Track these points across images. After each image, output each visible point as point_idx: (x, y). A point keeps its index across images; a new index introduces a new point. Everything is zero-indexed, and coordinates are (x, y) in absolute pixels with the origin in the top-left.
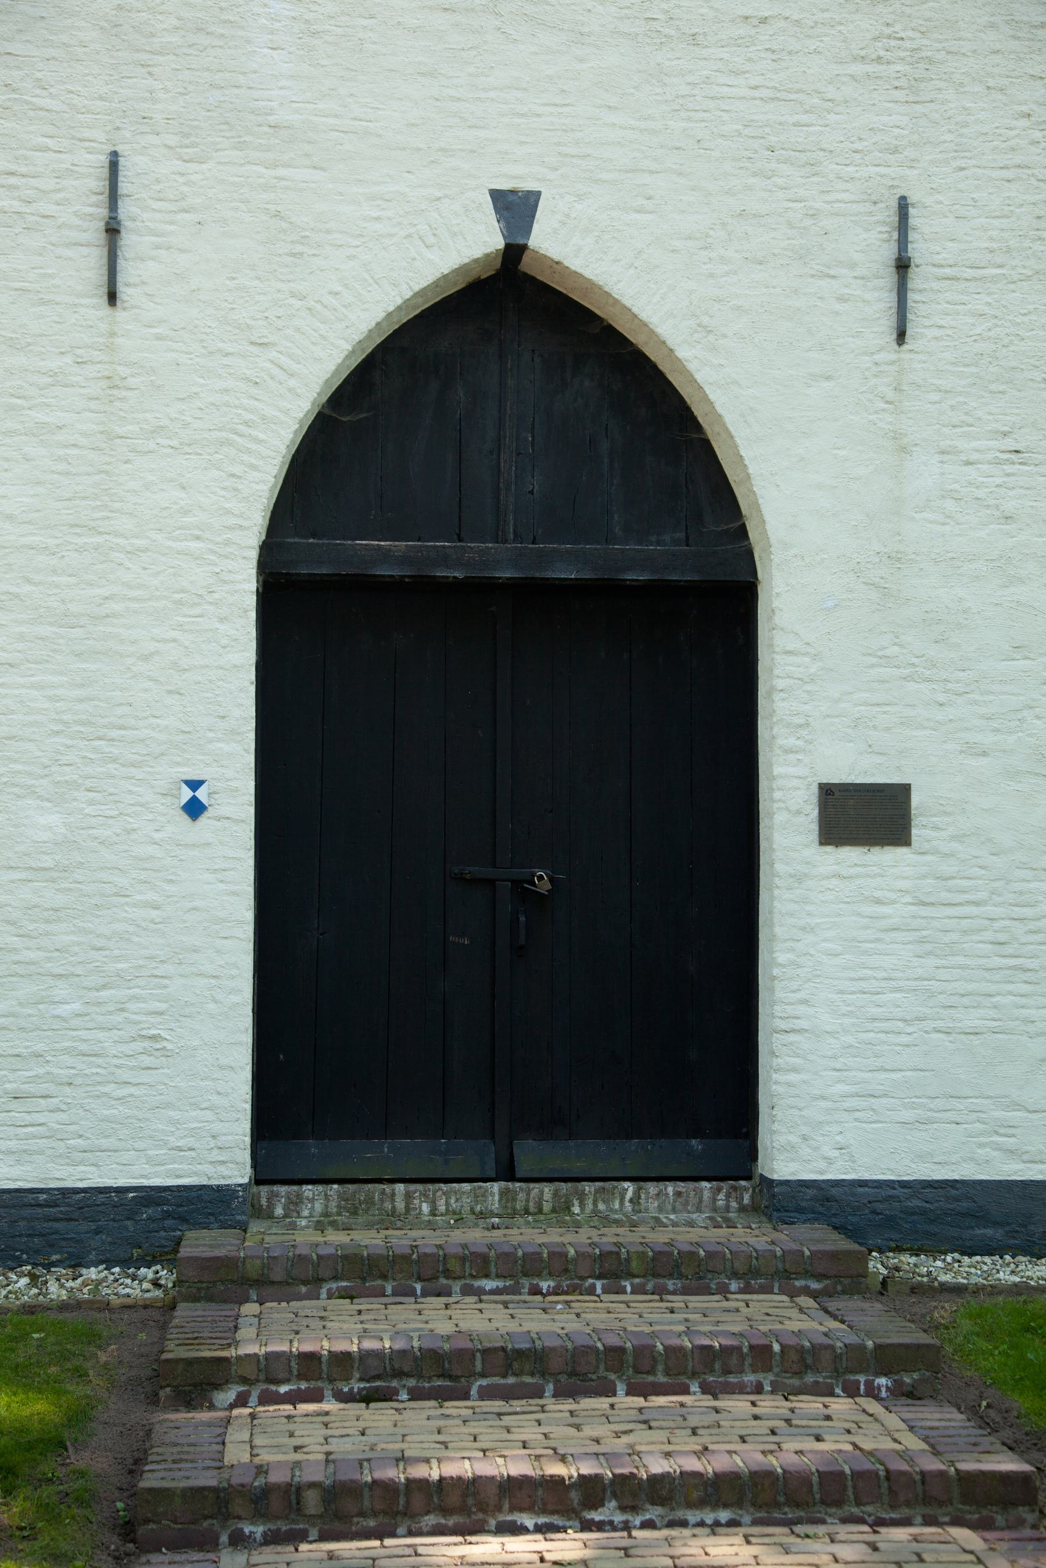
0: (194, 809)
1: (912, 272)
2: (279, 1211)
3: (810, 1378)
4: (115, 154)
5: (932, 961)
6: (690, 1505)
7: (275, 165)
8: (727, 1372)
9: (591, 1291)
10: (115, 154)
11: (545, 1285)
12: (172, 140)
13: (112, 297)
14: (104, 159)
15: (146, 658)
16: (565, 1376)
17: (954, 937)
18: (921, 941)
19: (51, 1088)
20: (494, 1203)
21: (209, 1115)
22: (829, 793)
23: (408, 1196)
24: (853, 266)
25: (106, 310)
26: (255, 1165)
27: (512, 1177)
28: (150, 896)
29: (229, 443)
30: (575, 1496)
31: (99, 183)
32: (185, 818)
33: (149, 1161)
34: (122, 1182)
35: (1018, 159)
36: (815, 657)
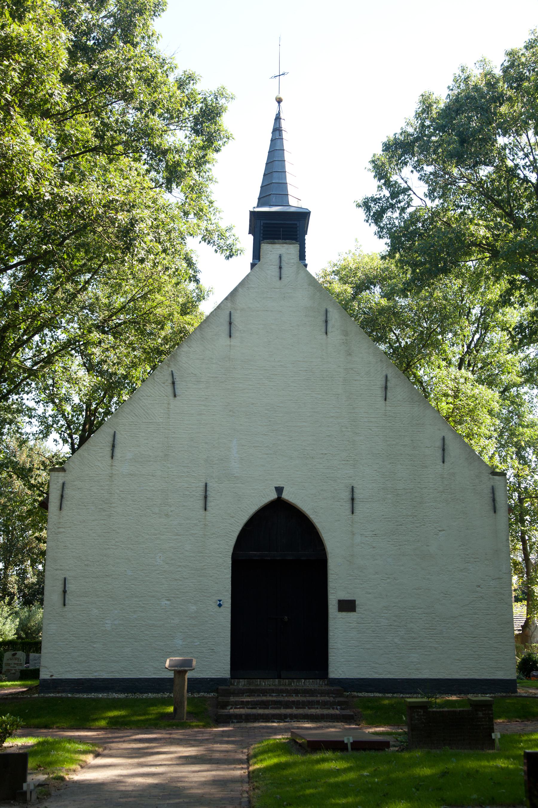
0: (220, 605)
1: (355, 500)
2: (236, 684)
3: (326, 706)
4: (206, 483)
6: (301, 719)
7: (235, 484)
9: (293, 696)
10: (206, 483)
12: (216, 480)
13: (205, 509)
14: (204, 484)
15: (211, 577)
16: (48, 194)
17: (365, 630)
21: (223, 664)
23: (260, 682)
24: (343, 499)
25: (204, 512)
26: (231, 675)
27: (281, 679)
28: (212, 622)
29: (226, 536)
31: (203, 488)
32: (218, 607)
33: (212, 673)
34: (207, 677)
35: (374, 479)
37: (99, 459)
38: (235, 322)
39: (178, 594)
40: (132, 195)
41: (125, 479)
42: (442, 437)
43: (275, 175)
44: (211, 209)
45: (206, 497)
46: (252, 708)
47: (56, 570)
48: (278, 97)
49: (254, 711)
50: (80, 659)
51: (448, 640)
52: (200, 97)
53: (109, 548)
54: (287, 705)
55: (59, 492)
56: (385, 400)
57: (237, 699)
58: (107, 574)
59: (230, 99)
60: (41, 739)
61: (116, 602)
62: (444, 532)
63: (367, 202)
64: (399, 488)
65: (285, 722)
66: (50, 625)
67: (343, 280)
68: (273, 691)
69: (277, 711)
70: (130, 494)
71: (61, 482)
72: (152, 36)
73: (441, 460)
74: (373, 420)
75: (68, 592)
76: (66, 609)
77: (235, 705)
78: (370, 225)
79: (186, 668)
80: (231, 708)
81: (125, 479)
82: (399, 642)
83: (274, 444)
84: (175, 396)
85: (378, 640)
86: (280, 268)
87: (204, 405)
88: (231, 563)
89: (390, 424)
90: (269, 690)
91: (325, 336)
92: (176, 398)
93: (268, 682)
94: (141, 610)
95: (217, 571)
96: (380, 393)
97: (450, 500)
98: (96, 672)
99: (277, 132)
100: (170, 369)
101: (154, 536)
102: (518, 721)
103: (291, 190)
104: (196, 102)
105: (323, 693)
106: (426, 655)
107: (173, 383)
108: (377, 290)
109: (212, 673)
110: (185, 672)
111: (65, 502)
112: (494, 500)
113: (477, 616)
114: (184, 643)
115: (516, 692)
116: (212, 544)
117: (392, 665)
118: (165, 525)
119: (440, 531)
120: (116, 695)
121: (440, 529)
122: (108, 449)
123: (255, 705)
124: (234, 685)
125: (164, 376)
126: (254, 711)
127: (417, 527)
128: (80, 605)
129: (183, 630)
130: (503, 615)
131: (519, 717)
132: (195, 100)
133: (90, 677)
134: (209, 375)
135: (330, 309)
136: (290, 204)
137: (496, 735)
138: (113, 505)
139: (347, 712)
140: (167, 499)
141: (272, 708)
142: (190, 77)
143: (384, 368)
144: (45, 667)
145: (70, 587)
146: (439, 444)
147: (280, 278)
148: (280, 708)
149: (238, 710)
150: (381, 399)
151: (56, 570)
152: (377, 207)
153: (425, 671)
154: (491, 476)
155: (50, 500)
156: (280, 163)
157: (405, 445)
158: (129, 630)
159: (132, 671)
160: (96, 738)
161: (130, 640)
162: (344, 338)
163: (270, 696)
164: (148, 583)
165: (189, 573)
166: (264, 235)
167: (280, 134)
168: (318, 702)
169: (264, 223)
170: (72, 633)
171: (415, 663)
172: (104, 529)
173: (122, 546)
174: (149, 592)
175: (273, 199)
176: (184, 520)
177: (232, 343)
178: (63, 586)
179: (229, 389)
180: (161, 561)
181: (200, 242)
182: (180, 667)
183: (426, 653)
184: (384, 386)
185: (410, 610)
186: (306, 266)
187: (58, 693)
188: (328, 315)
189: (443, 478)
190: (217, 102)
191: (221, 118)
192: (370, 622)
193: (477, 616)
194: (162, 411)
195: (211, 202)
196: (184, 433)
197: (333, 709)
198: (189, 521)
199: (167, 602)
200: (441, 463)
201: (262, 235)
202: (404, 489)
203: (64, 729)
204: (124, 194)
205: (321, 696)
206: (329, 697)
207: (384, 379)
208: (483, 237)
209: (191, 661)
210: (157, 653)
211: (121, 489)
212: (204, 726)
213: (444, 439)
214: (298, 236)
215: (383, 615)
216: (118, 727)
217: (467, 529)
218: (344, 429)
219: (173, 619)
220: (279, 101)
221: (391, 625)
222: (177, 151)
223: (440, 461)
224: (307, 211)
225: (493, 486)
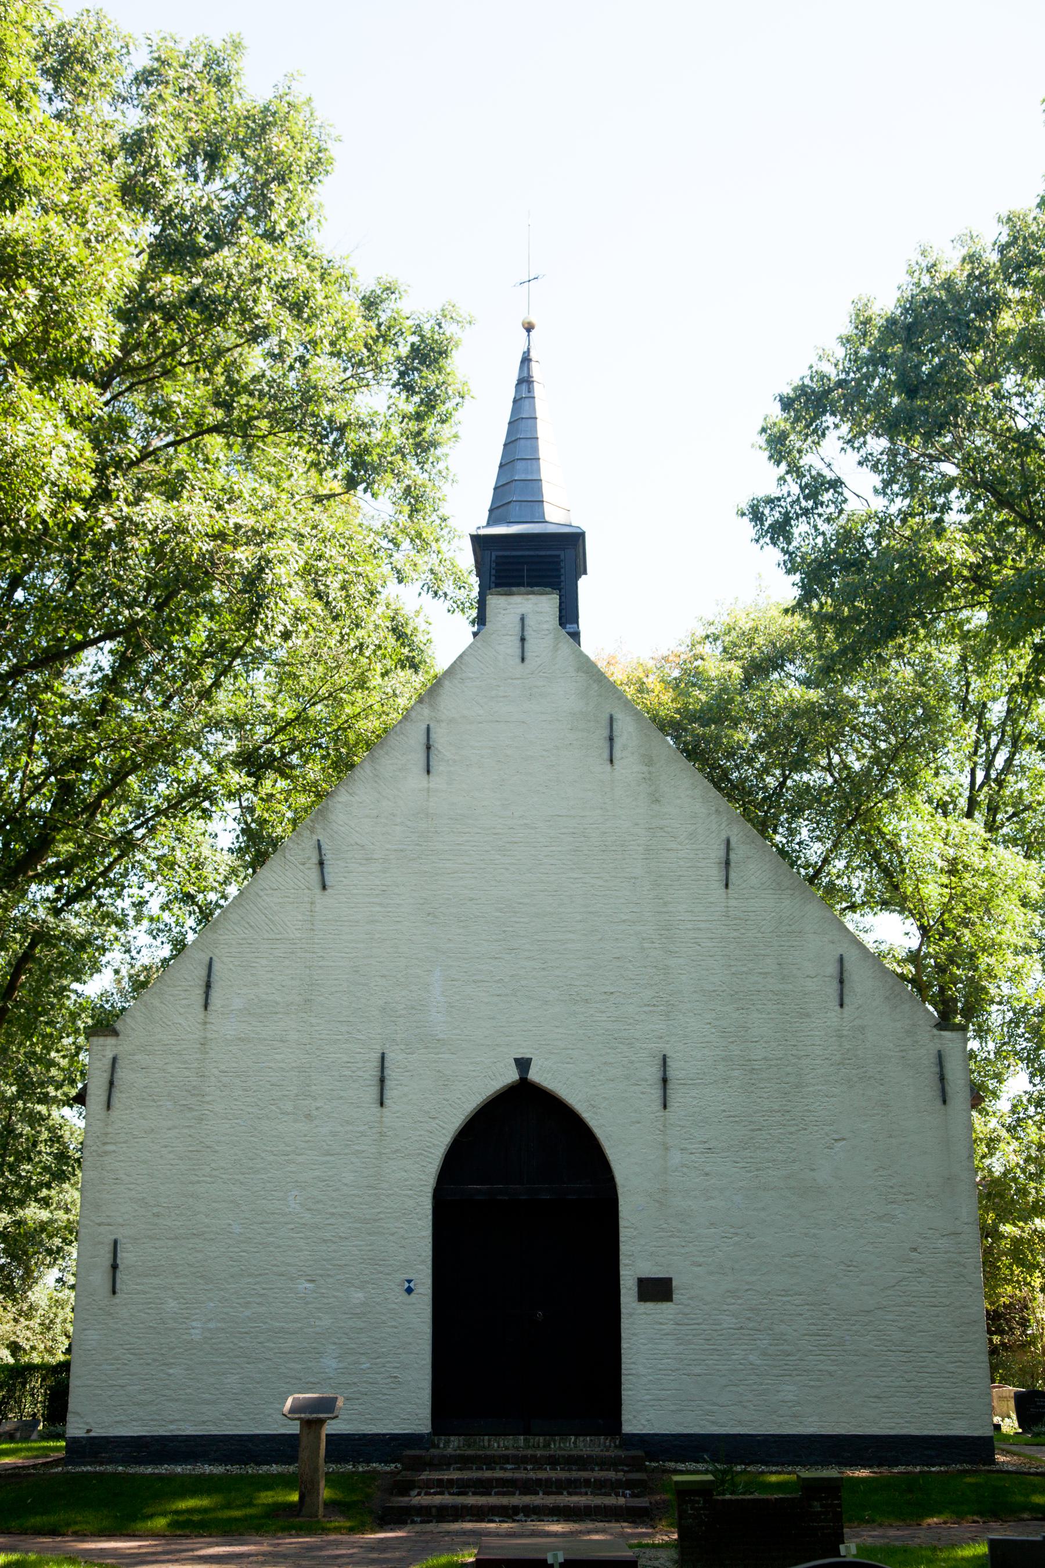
0: (409, 1291)
2: (442, 1445)
4: (383, 1054)
5: (682, 1347)
8: (576, 1488)
9: (545, 1469)
10: (383, 1054)
11: (529, 1467)
12: (403, 1047)
13: (382, 1104)
14: (379, 1055)
15: (393, 1234)
17: (690, 1337)
18: (678, 1339)
19: (358, 1395)
20: (521, 1443)
22: (642, 1282)
23: (489, 1441)
24: (647, 1080)
25: (379, 1109)
28: (394, 1323)
29: (421, 1154)
30: (510, 1512)
31: (377, 1064)
33: (394, 1423)
34: (385, 1432)
36: (636, 1229)
37: (182, 1011)
38: (436, 745)
39: (329, 1270)
40: (270, 515)
41: (230, 1048)
42: (838, 956)
43: (520, 465)
44: (444, 532)
45: (382, 1080)
46: (459, 1494)
47: (99, 1225)
48: (528, 320)
49: (460, 1500)
50: (143, 1397)
51: (855, 1358)
52: (410, 323)
53: (198, 1182)
54: (528, 1487)
55: (106, 1076)
56: (727, 886)
57: (436, 1476)
58: (195, 1232)
59: (467, 326)
60: (14, 1557)
61: (210, 1286)
62: (843, 1143)
63: (757, 506)
64: (755, 1058)
65: (514, 1521)
66: (87, 1332)
67: (729, 655)
68: (506, 1459)
69: (504, 1501)
70: (239, 1076)
71: (110, 1055)
72: (308, 219)
73: (837, 1002)
74: (703, 925)
75: (121, 1267)
76: (117, 1301)
77: (427, 1487)
78: (762, 547)
79: (321, 1416)
80: (419, 1494)
81: (230, 1048)
82: (758, 1362)
83: (512, 976)
84: (324, 887)
85: (717, 1357)
86: (523, 640)
87: (381, 905)
88: (430, 1207)
89: (735, 934)
90: (500, 1457)
91: (609, 765)
92: (326, 893)
93: (509, 1441)
94: (259, 1300)
95: (404, 1223)
96: (715, 873)
97: (855, 1079)
98: (172, 1422)
99: (524, 386)
100: (315, 837)
101: (283, 1158)
102: (978, 1522)
103: (549, 492)
104: (403, 333)
105: (604, 1463)
106: (812, 1387)
107: (321, 863)
108: (796, 669)
109: (394, 1423)
110: (321, 1422)
111: (117, 1095)
112: (942, 1078)
113: (911, 1309)
114: (341, 1365)
115: (993, 1462)
116: (393, 1171)
117: (745, 1407)
118: (305, 1136)
119: (836, 1140)
120: (208, 1469)
121: (836, 1137)
122: (200, 991)
123: (463, 1487)
124: (438, 1447)
125: (303, 850)
126: (460, 1500)
127: (791, 1133)
128: (145, 1293)
129: (339, 1338)
130: (964, 1307)
131: (981, 1514)
132: (400, 330)
133: (162, 1432)
134: (388, 846)
135: (618, 716)
136: (547, 518)
137: (848, 1548)
138: (208, 1098)
139: (643, 1502)
140: (308, 1086)
141: (497, 1494)
142: (388, 289)
143: (724, 825)
144: (78, 1414)
145: (126, 1258)
146: (832, 969)
147: (523, 660)
148: (513, 1494)
149: (430, 1497)
150: (718, 886)
151: (99, 1225)
152: (777, 515)
153: (810, 1419)
154: (935, 1032)
155: (89, 1092)
156: (529, 442)
157: (766, 973)
158: (235, 1341)
159: (240, 1421)
160: (132, 1554)
161: (237, 1360)
162: (645, 769)
163: (502, 1469)
164: (272, 1249)
165: (350, 1228)
166: (497, 577)
167: (530, 390)
168: (587, 1482)
169: (497, 557)
170: (129, 1346)
171: (790, 1404)
172: (190, 1145)
173: (224, 1176)
174: (275, 1265)
175: (515, 510)
176: (342, 1126)
177: (432, 785)
178: (111, 1255)
179: (426, 872)
180: (297, 1206)
181: (420, 594)
182: (311, 1413)
183: (812, 1383)
184: (723, 860)
185: (780, 1298)
186: (575, 636)
187: (101, 1464)
188: (615, 727)
189: (841, 1037)
190: (441, 331)
191: (449, 361)
192: (700, 1321)
193: (911, 1309)
194: (300, 918)
195: (444, 520)
196: (343, 957)
197: (617, 1495)
198: (350, 1128)
199: (308, 1285)
200: (838, 1008)
201: (493, 578)
202: (765, 1058)
203: (82, 1536)
204: (255, 512)
205: (601, 1470)
206: (617, 1471)
207: (723, 846)
208: (963, 565)
209: (334, 1400)
210: (288, 1386)
211: (223, 1068)
212: (351, 1530)
213: (841, 960)
214: (563, 578)
215: (725, 1307)
216: (187, 1532)
217: (890, 1136)
218: (646, 945)
219: (320, 1319)
220: (529, 328)
221: (741, 1328)
222: (363, 426)
223: (834, 1003)
224: (579, 531)
225: (939, 1051)
